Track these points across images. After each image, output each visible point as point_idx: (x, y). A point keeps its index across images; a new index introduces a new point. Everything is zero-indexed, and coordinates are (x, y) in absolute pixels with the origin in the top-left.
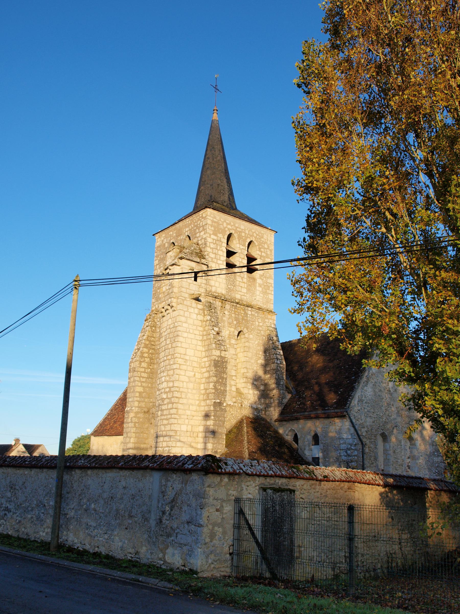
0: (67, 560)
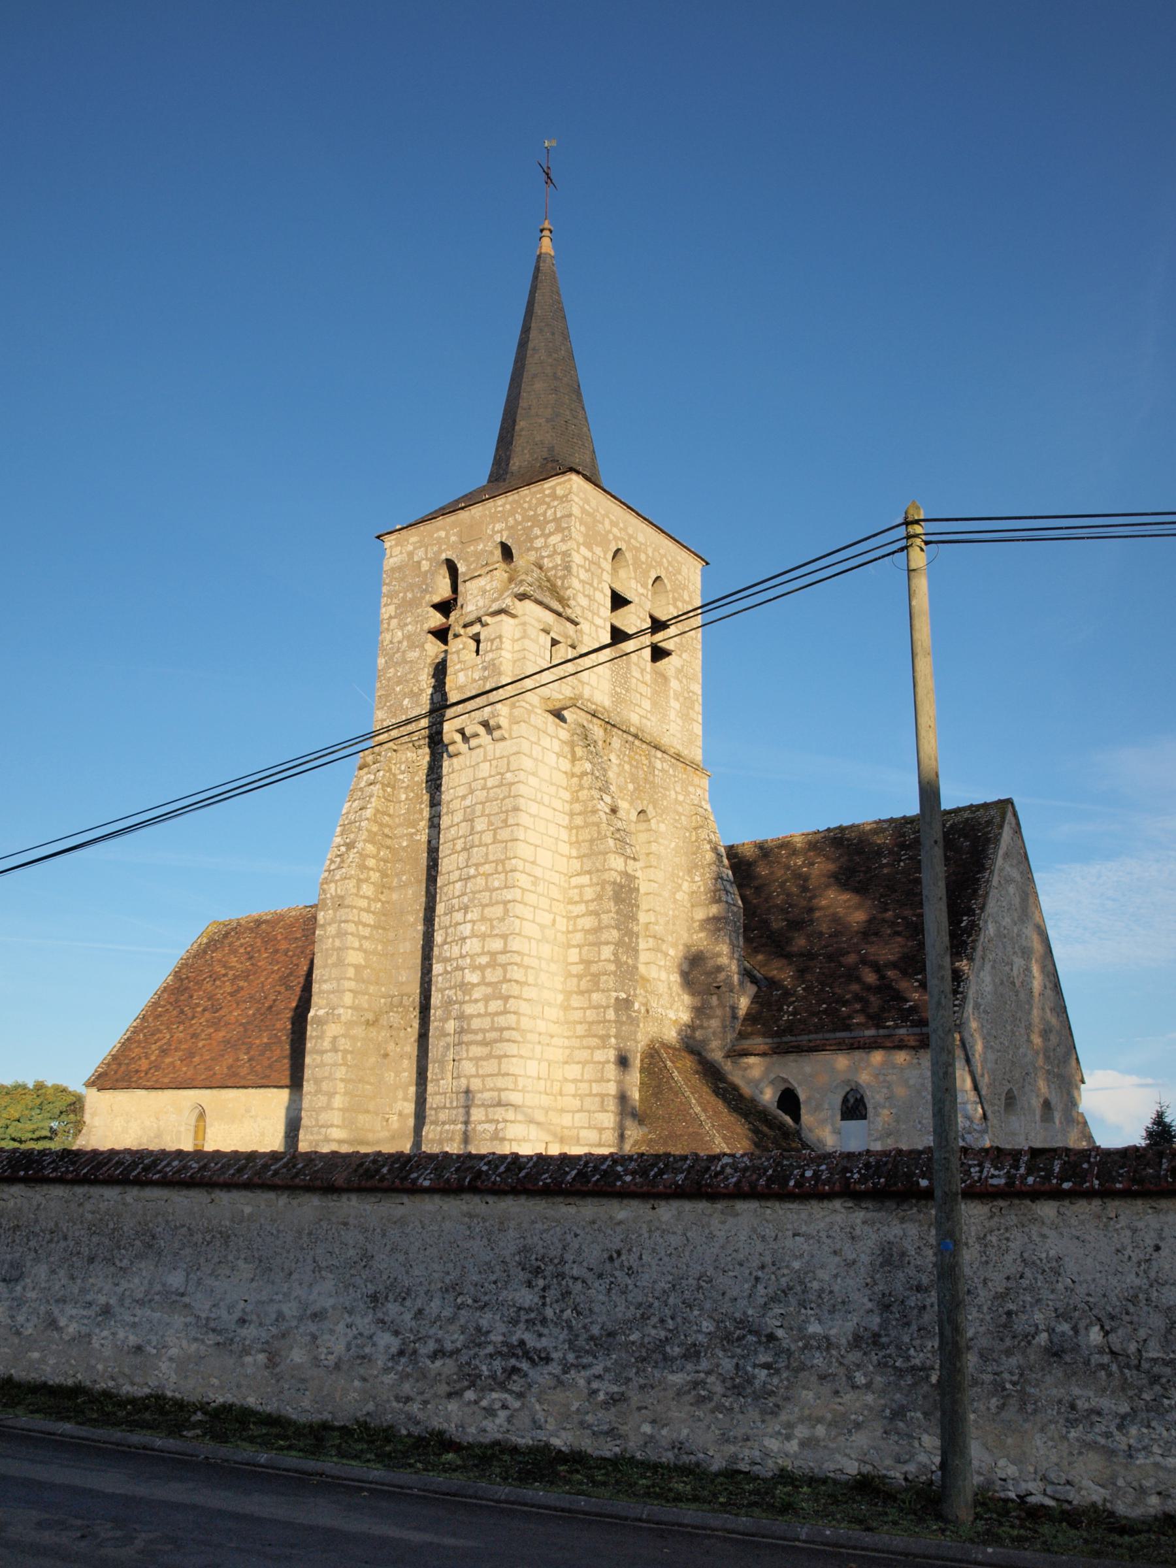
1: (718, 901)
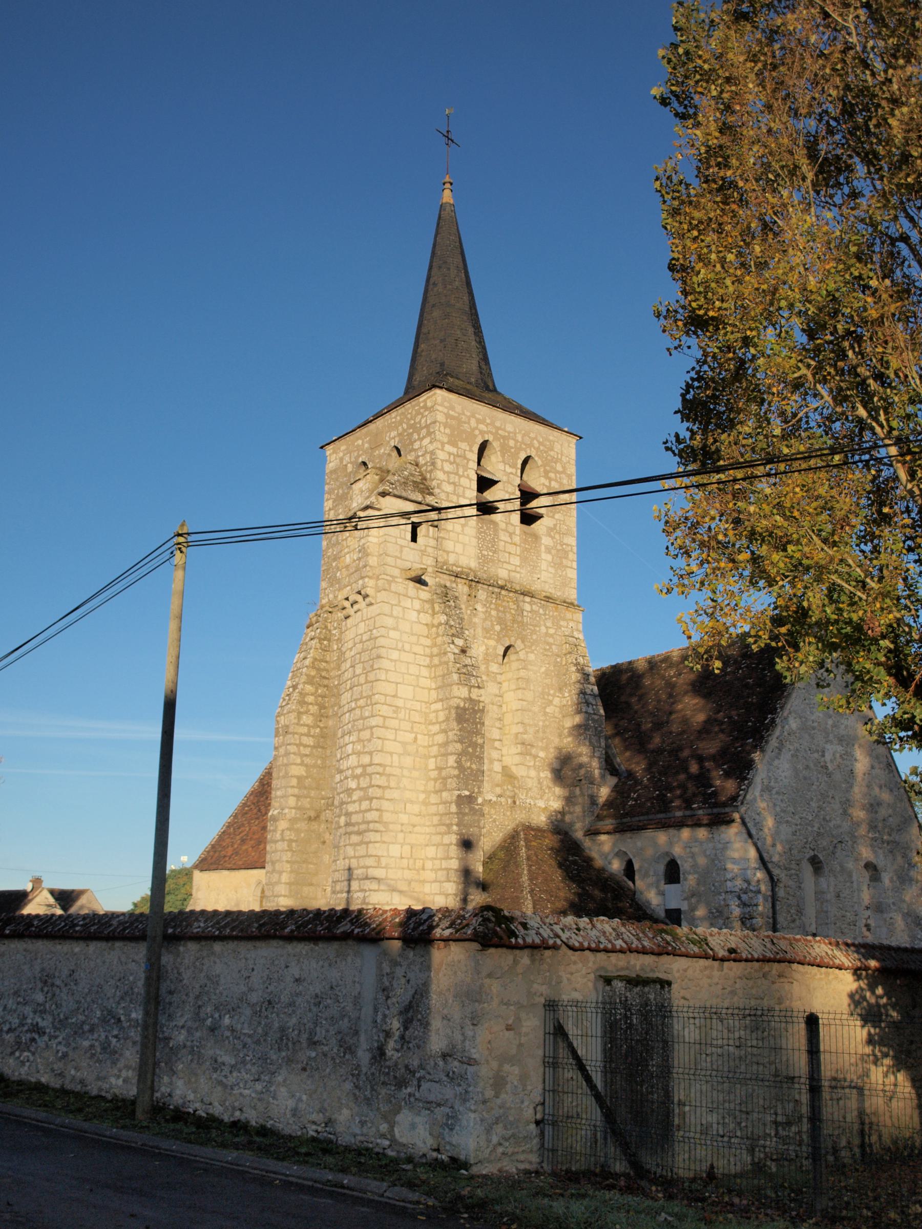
0: (177, 1139)
1: (579, 712)
